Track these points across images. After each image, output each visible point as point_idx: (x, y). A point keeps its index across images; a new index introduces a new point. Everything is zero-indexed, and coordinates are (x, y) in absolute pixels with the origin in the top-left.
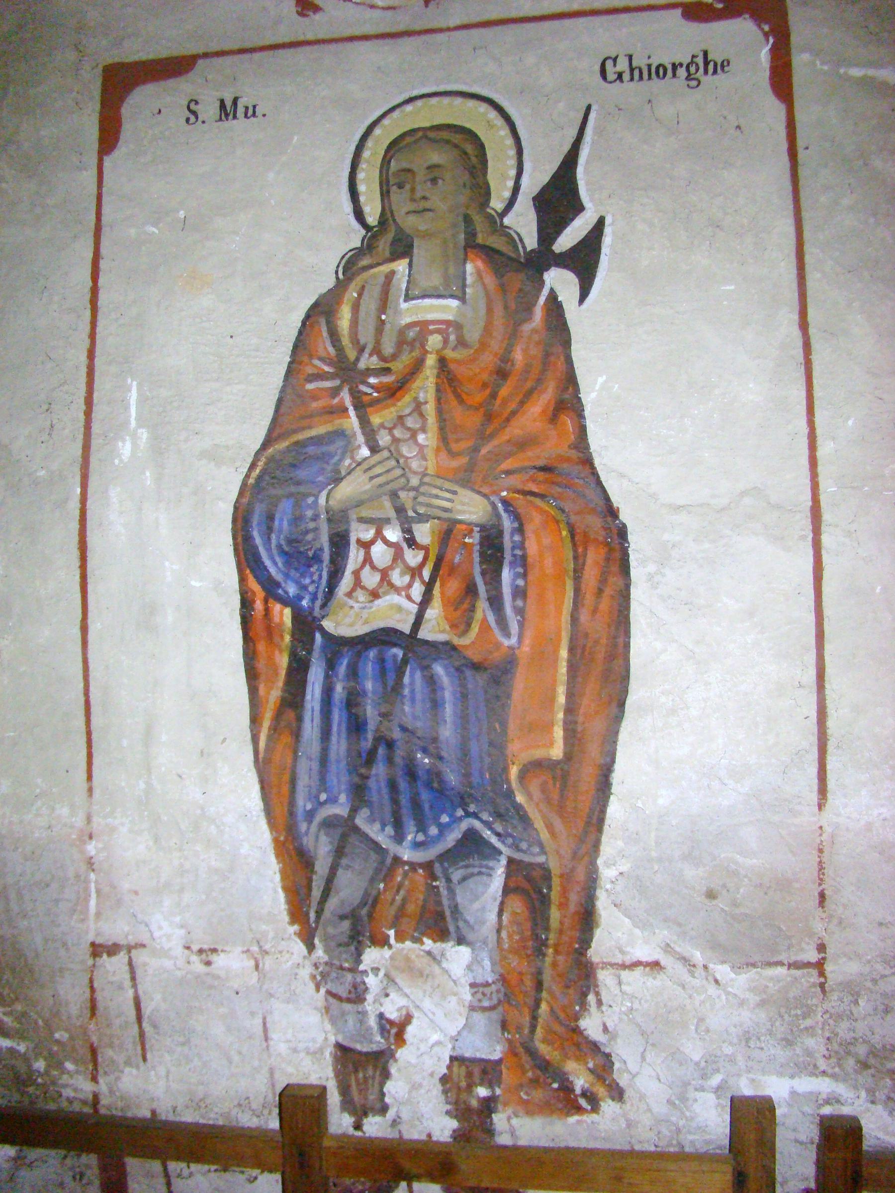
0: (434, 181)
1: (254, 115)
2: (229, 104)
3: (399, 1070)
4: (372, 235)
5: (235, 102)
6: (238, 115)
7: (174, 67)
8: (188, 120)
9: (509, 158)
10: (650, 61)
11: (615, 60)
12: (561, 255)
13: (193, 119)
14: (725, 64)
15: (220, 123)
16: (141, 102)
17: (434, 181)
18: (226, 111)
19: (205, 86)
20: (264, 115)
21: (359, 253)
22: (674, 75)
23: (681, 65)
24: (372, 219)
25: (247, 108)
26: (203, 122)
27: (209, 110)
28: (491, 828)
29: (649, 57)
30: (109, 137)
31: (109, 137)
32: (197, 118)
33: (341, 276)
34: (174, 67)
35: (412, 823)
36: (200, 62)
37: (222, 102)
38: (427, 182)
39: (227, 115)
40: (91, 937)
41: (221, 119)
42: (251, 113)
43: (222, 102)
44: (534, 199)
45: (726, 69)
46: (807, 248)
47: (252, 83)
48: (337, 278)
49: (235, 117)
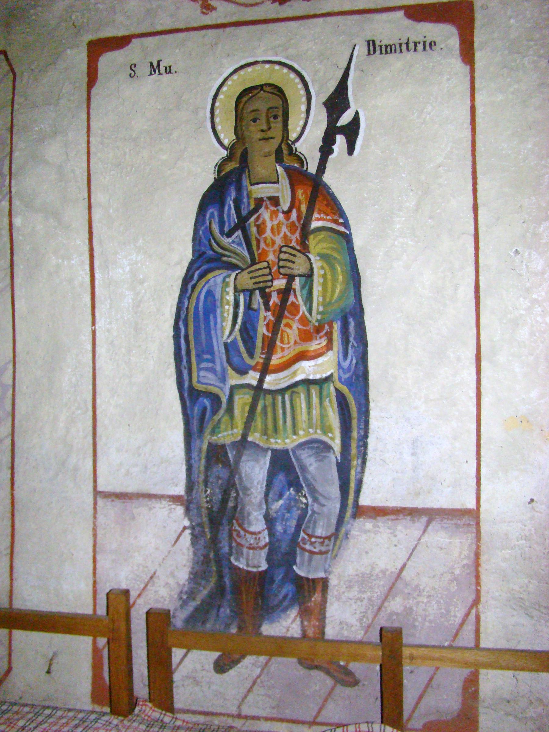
1: (170, 72)
2: (155, 65)
3: (484, 607)
5: (159, 62)
7: (120, 42)
9: (297, 84)
10: (425, 39)
12: (342, 127)
14: (433, 44)
15: (152, 76)
16: (108, 61)
18: (155, 68)
19: (133, 52)
22: (415, 50)
27: (143, 69)
29: (380, 42)
34: (120, 42)
37: (151, 64)
39: (155, 71)
41: (151, 74)
42: (169, 70)
43: (151, 64)
44: (325, 104)
45: (433, 48)
46: (157, 38)
47: (170, 51)
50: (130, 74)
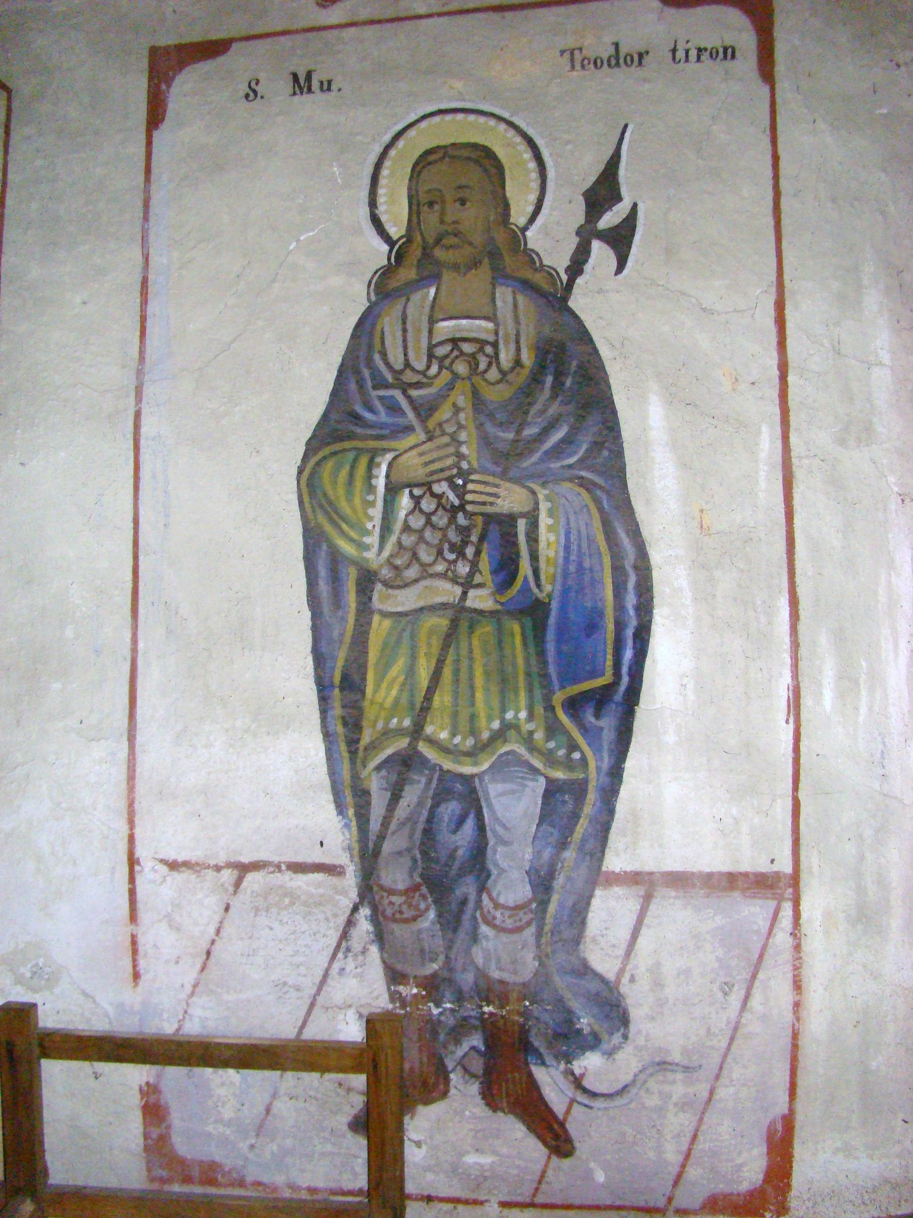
0: (463, 202)
1: (329, 89)
4: (400, 252)
6: (313, 89)
7: (213, 49)
8: (247, 96)
11: (581, 49)
13: (252, 95)
16: (184, 88)
17: (463, 202)
18: (302, 84)
20: (339, 90)
21: (387, 272)
23: (706, 50)
24: (395, 232)
25: (322, 83)
26: (262, 97)
28: (605, 651)
30: (155, 116)
31: (155, 116)
32: (256, 95)
33: (373, 298)
35: (601, 1172)
36: (766, 90)
38: (449, 216)
40: (438, 225)
41: (295, 94)
42: (326, 86)
43: (295, 77)
48: (369, 299)
49: (310, 90)
50: (257, 84)
